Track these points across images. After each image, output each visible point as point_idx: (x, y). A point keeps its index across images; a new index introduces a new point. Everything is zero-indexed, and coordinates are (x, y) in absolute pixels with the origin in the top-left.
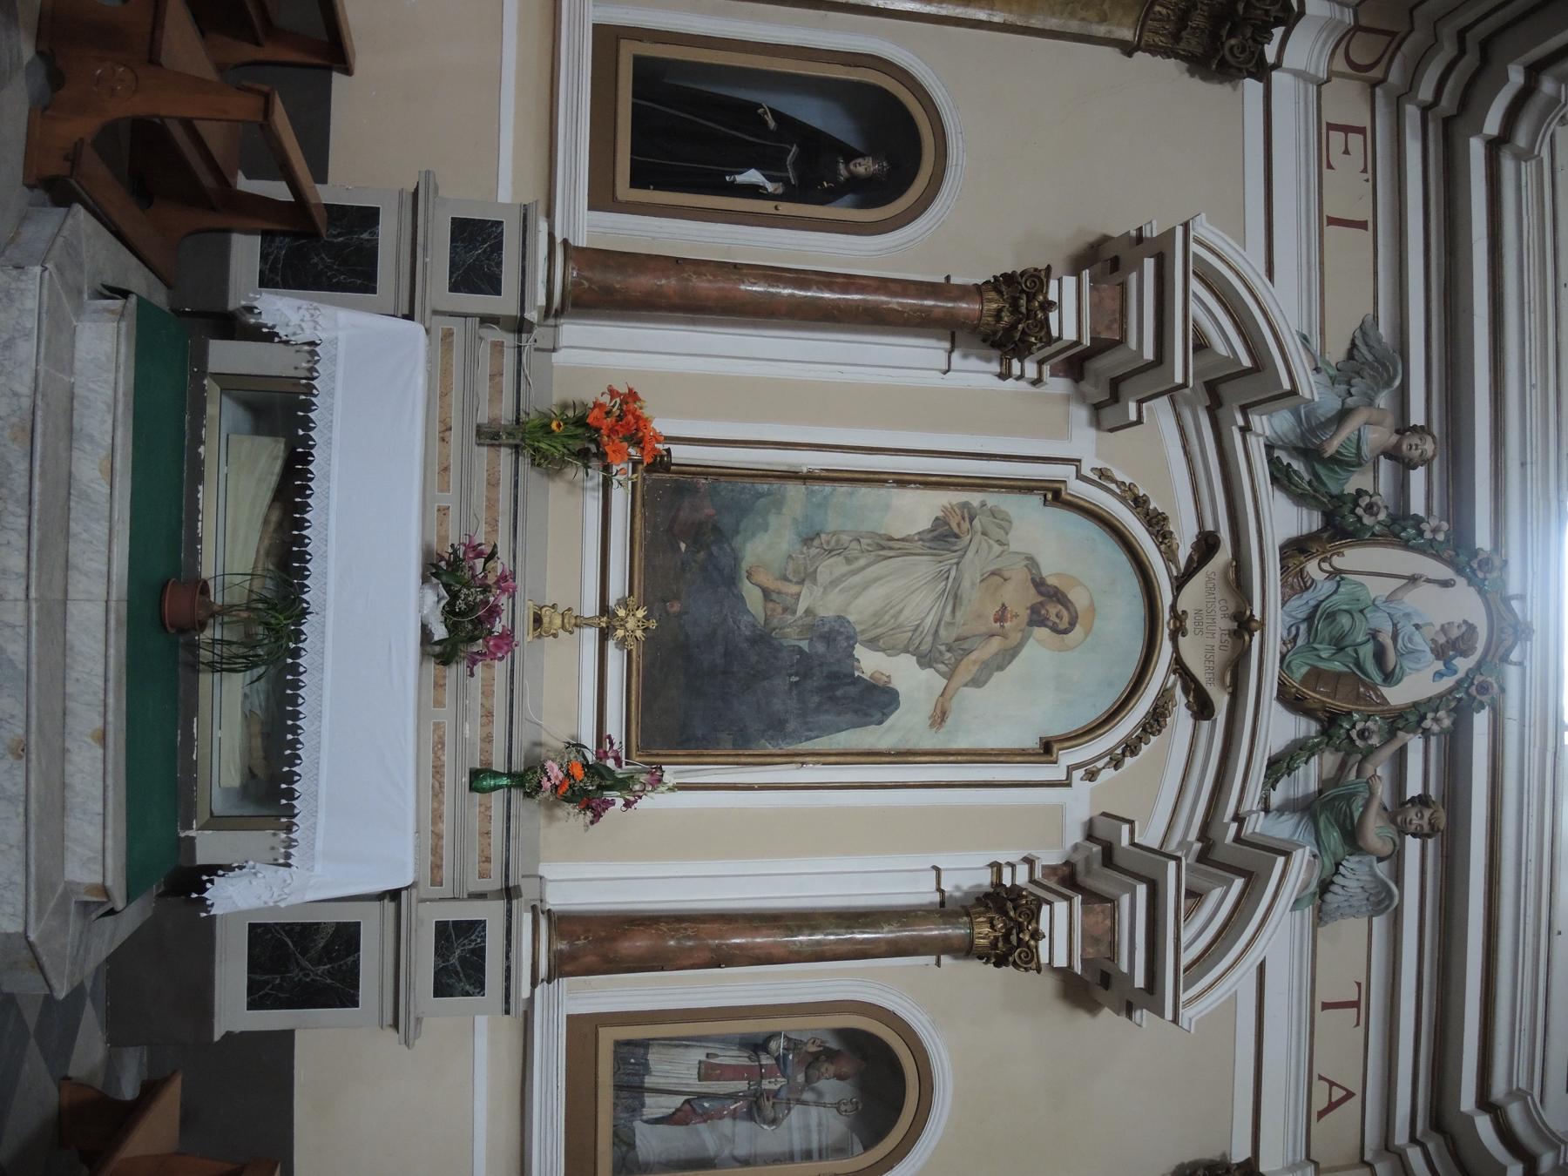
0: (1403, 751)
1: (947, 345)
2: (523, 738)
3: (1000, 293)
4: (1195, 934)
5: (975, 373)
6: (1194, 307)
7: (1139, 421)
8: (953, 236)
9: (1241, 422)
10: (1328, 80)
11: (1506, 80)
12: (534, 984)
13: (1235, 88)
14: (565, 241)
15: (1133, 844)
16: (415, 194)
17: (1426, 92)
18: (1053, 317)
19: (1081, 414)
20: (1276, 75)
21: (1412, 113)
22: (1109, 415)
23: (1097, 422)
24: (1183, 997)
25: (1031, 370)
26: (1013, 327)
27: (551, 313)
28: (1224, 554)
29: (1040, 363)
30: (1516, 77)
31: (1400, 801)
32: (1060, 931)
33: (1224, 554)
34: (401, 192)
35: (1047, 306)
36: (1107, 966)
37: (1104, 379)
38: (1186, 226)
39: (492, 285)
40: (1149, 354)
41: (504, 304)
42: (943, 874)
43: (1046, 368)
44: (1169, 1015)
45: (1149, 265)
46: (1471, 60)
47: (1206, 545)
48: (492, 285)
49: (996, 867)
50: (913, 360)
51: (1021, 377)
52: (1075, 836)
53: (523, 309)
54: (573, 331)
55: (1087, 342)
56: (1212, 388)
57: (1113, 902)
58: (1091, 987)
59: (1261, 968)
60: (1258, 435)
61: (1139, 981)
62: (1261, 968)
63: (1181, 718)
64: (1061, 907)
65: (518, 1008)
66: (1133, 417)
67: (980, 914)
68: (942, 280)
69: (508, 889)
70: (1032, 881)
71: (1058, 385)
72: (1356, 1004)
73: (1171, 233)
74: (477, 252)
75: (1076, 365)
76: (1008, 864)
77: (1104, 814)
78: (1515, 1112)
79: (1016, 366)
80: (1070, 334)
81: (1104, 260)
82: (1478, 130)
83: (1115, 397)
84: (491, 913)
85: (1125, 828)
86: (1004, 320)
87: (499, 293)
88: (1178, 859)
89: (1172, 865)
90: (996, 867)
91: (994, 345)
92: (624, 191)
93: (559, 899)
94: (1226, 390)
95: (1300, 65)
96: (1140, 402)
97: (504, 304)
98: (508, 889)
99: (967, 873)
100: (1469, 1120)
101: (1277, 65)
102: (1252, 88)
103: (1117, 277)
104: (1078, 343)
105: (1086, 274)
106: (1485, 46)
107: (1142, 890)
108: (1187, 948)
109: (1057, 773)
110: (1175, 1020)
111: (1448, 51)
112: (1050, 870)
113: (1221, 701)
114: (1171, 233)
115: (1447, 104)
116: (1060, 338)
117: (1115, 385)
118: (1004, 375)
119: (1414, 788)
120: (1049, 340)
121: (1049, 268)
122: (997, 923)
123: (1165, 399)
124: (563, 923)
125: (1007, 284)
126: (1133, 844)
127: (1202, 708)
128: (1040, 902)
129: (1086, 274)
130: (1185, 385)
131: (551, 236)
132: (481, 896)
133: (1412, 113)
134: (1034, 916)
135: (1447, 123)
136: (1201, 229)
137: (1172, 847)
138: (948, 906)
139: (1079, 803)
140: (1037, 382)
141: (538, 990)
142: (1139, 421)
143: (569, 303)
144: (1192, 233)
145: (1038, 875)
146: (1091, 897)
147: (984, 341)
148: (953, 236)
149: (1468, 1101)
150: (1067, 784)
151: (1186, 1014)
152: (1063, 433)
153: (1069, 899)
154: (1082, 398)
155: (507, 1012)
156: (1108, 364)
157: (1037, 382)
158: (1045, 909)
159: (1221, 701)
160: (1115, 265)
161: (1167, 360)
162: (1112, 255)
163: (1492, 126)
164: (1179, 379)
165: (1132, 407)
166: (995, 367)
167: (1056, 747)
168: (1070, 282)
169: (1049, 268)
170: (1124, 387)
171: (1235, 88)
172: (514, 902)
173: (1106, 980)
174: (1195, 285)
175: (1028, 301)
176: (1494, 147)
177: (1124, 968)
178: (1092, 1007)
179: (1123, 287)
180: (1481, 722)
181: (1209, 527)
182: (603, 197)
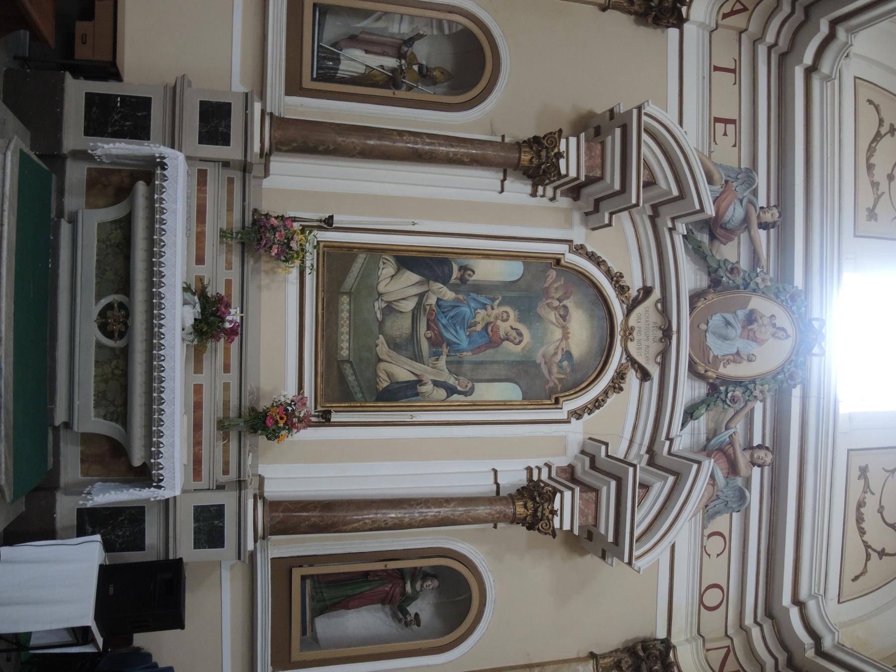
0: (752, 410)
1: (501, 176)
2: (246, 403)
3: (531, 148)
4: (644, 516)
5: (518, 191)
6: (644, 149)
7: (610, 225)
8: (504, 112)
9: (670, 225)
10: (716, 29)
11: (818, 30)
12: (255, 541)
13: (663, 32)
14: (271, 114)
15: (607, 456)
16: (175, 88)
17: (770, 38)
18: (562, 162)
19: (577, 217)
20: (686, 26)
21: (762, 50)
22: (594, 220)
23: (585, 223)
24: (636, 553)
25: (550, 192)
26: (539, 167)
27: (265, 156)
28: (657, 294)
29: (555, 188)
30: (824, 29)
31: (749, 447)
32: (567, 509)
33: (657, 294)
34: (166, 87)
35: (559, 155)
36: (593, 529)
37: (592, 199)
38: (639, 108)
39: (225, 140)
40: (617, 187)
41: (232, 152)
42: (499, 474)
43: (558, 192)
44: (626, 560)
45: (618, 132)
46: (799, 15)
47: (647, 291)
48: (225, 140)
49: (529, 470)
50: (479, 185)
51: (543, 196)
52: (573, 450)
53: (246, 156)
54: (278, 163)
55: (583, 178)
56: (655, 207)
57: (597, 491)
58: (585, 541)
59: (673, 547)
60: (679, 234)
61: (611, 539)
62: (673, 547)
63: (632, 379)
64: (568, 494)
65: (245, 557)
66: (607, 221)
67: (519, 500)
68: (499, 139)
69: (240, 482)
70: (550, 477)
71: (564, 202)
72: (708, 650)
73: (630, 112)
74: (215, 121)
75: (575, 191)
76: (537, 467)
77: (590, 439)
78: (811, 606)
79: (540, 189)
80: (573, 174)
81: (594, 127)
82: (800, 61)
83: (597, 209)
84: (227, 499)
85: (603, 447)
86: (533, 161)
87: (228, 145)
88: (634, 466)
89: (631, 469)
90: (529, 470)
91: (530, 177)
92: (307, 83)
93: (272, 491)
94: (662, 209)
95: (701, 19)
96: (611, 214)
97: (232, 152)
98: (240, 482)
99: (513, 476)
100: (787, 610)
101: (687, 20)
102: (673, 32)
103: (600, 139)
104: (577, 178)
105: (582, 136)
106: (807, 9)
107: (613, 484)
108: (638, 525)
109: (563, 415)
110: (630, 563)
111: (786, 9)
112: (561, 470)
113: (655, 372)
114: (630, 112)
115: (783, 44)
116: (567, 175)
117: (597, 202)
118: (534, 194)
119: (757, 441)
120: (559, 176)
121: (560, 131)
122: (531, 505)
123: (626, 213)
124: (273, 506)
125: (535, 142)
126: (607, 456)
127: (645, 376)
128: (555, 491)
129: (582, 136)
130: (637, 205)
131: (263, 112)
132: (220, 487)
133: (762, 50)
134: (552, 500)
135: (783, 57)
136: (649, 109)
137: (631, 458)
138: (502, 494)
139: (575, 433)
140: (553, 199)
141: (258, 544)
142: (610, 225)
143: (274, 148)
144: (643, 111)
145: (553, 475)
146: (586, 488)
147: (524, 174)
148: (504, 112)
149: (786, 600)
150: (567, 422)
151: (637, 564)
152: (570, 224)
153: (573, 490)
154: (579, 209)
155: (239, 558)
156: (594, 191)
157: (553, 199)
158: (558, 495)
159: (655, 372)
160: (598, 131)
161: (627, 190)
162: (595, 125)
163: (808, 59)
164: (634, 201)
165: (607, 216)
166: (529, 189)
167: (561, 400)
168: (573, 141)
169: (560, 131)
170: (603, 205)
171: (663, 32)
172: (243, 492)
173: (590, 536)
174: (645, 137)
175: (548, 153)
176: (809, 72)
177: (602, 531)
178: (583, 552)
179: (603, 144)
180: (796, 393)
181: (649, 284)
182: (294, 87)
